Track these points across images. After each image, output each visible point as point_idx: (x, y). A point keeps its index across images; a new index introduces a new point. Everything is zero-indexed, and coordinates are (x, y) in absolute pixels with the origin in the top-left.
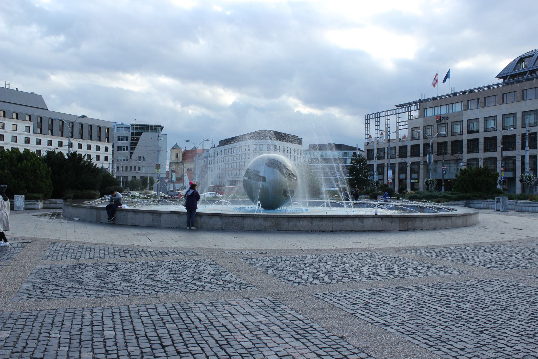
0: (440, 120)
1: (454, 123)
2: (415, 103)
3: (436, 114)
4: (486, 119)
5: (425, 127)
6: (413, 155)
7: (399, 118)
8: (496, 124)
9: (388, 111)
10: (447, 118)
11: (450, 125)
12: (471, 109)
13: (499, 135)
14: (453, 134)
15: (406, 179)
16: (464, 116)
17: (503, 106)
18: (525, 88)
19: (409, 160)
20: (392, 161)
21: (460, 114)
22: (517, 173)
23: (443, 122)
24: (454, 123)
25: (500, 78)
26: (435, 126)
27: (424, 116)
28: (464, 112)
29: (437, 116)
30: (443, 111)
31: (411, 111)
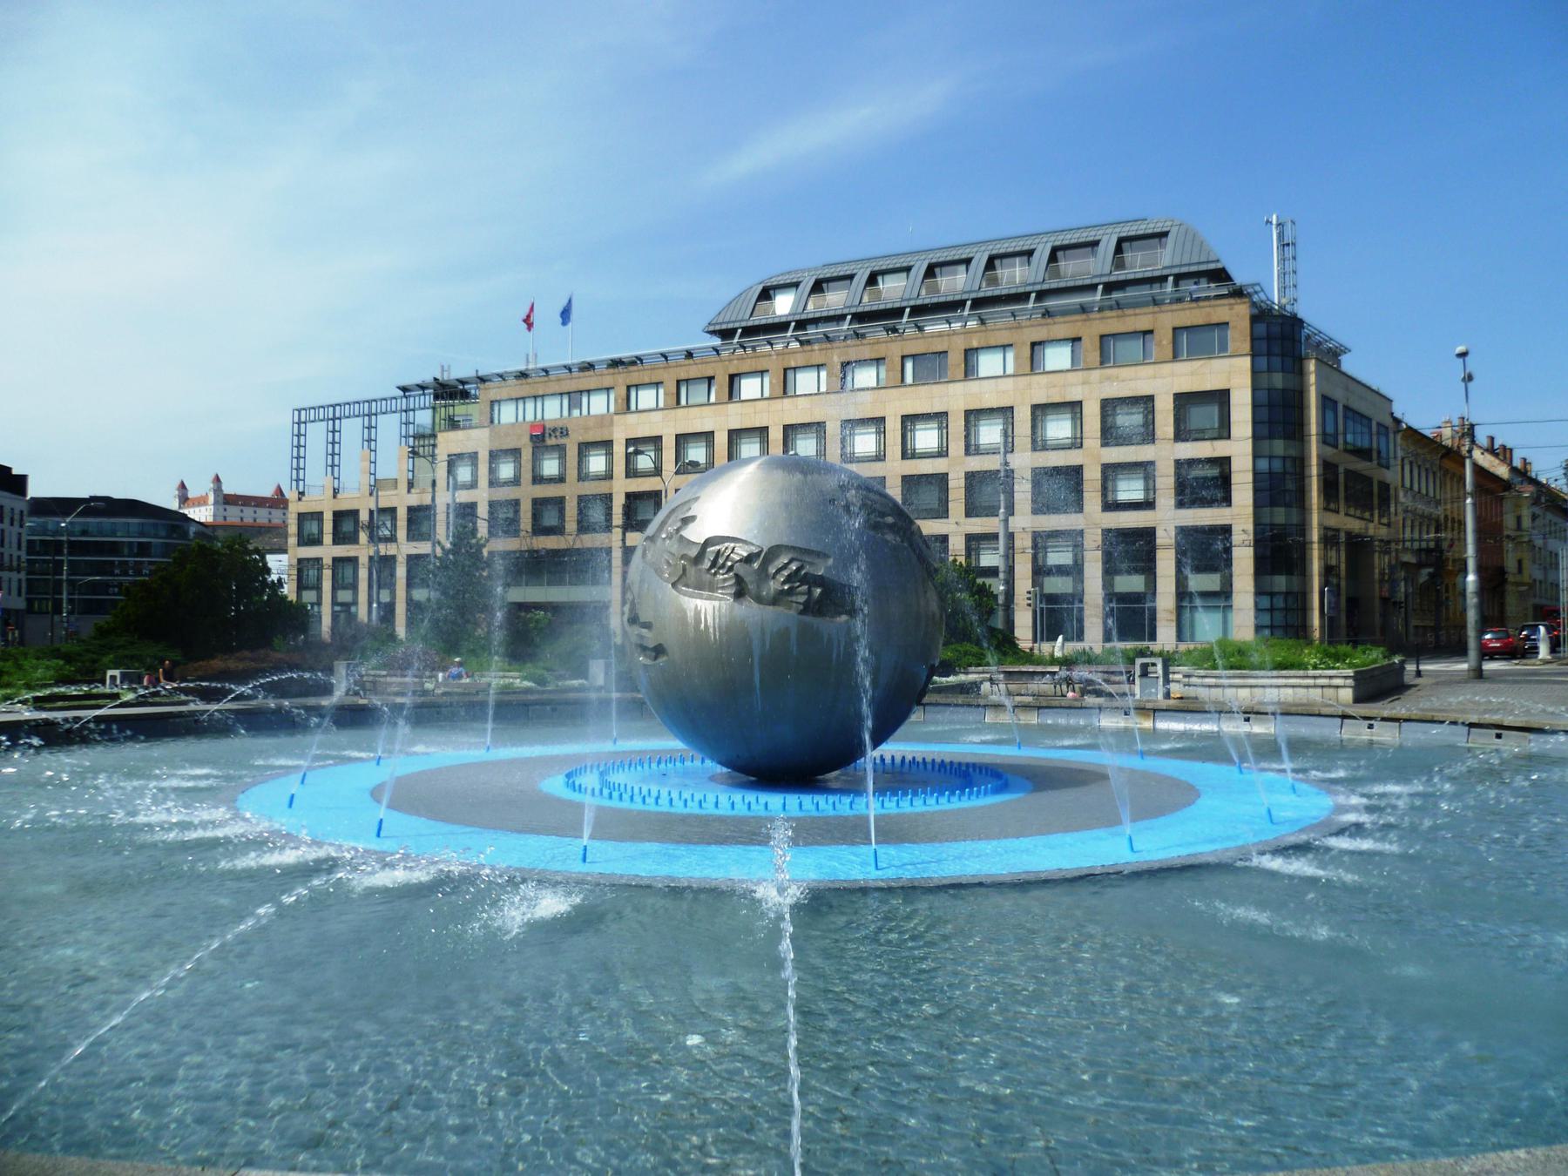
0: (543, 439)
1: (585, 448)
2: (422, 387)
3: (530, 417)
4: (682, 440)
5: (494, 456)
6: (339, 539)
7: (369, 428)
8: (475, 474)
9: (334, 406)
10: (564, 432)
11: (572, 452)
12: (687, 406)
13: (957, 468)
14: (538, 479)
15: (355, 603)
16: (616, 429)
17: (731, 406)
18: (793, 364)
19: (328, 551)
20: (343, 551)
21: (604, 421)
22: (1173, 589)
23: (551, 441)
24: (585, 448)
25: (713, 333)
26: (527, 455)
27: (492, 421)
28: (616, 418)
29: (533, 426)
30: (553, 410)
31: (369, 415)
